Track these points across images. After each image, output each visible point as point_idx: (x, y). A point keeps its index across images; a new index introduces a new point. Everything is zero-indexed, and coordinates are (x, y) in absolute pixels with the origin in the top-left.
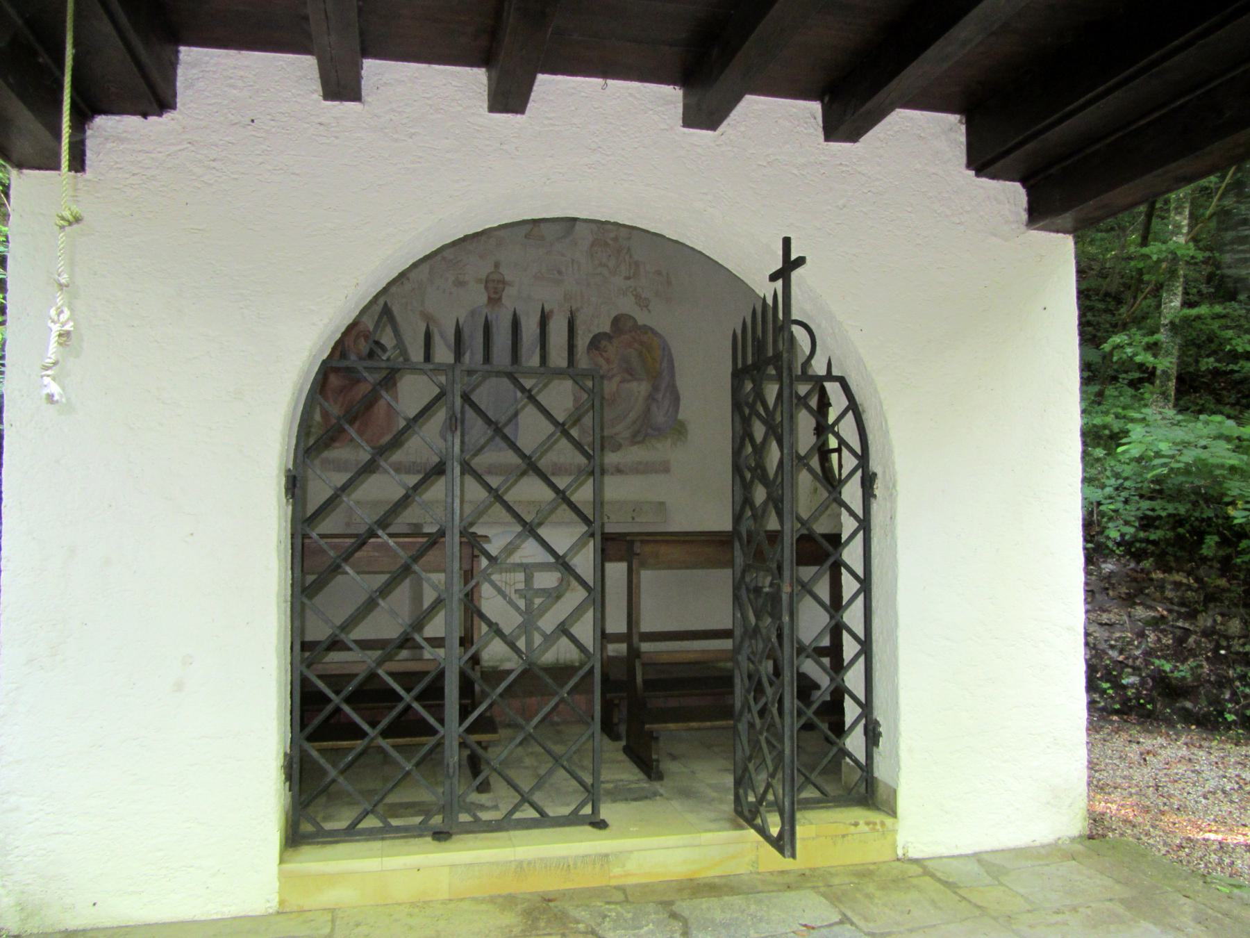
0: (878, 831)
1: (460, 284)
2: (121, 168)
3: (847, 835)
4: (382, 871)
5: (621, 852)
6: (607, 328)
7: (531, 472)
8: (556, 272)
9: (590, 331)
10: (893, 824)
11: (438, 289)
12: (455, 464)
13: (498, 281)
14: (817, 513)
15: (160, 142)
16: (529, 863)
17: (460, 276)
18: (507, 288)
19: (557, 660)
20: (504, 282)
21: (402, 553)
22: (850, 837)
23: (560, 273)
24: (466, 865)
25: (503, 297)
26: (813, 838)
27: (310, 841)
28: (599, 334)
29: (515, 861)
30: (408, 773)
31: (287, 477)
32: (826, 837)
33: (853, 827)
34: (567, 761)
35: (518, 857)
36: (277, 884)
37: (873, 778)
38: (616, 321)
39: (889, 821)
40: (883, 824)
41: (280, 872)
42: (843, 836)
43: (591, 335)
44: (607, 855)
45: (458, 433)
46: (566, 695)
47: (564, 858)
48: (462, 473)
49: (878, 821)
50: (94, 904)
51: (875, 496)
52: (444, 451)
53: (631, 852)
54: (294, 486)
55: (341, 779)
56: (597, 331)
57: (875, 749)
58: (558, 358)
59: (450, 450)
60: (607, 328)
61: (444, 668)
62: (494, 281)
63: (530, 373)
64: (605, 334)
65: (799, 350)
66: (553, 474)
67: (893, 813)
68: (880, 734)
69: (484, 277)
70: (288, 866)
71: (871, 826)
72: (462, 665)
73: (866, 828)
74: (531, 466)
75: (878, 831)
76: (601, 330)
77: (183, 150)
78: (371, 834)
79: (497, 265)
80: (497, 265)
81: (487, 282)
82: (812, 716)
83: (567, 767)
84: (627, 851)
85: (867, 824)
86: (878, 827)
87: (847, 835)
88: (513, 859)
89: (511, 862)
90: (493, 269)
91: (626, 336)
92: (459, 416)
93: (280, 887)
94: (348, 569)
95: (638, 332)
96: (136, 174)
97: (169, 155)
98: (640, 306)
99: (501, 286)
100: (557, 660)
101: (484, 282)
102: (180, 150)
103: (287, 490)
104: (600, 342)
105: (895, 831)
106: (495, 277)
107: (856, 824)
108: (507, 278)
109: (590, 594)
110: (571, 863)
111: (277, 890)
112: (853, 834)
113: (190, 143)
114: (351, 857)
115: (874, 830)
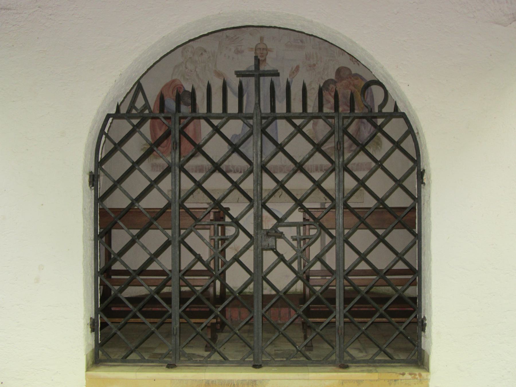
0: (417, 379)
1: (238, 52)
2: (8, 23)
3: (398, 380)
4: (136, 379)
5: (263, 380)
6: (333, 76)
7: (299, 171)
8: (299, 41)
9: (322, 79)
10: (427, 375)
11: (229, 57)
12: (176, 168)
13: (263, 49)
14: (413, 197)
15: (25, 8)
16: (213, 381)
17: (238, 47)
18: (269, 52)
19: (296, 290)
20: (267, 49)
21: (148, 216)
22: (399, 381)
23: (302, 41)
24: (179, 380)
25: (267, 58)
26: (377, 380)
27: (106, 363)
28: (328, 80)
29: (205, 380)
30: (153, 333)
31: (90, 176)
32: (385, 380)
33: (401, 376)
34: (239, 330)
35: (207, 378)
36: (85, 381)
37: (421, 349)
38: (339, 71)
39: (424, 374)
40: (420, 375)
41: (86, 375)
42: (395, 380)
43: (324, 81)
44: (255, 381)
45: (178, 151)
46: (238, 295)
47: (231, 380)
48: (180, 172)
49: (417, 373)
50: (2, 383)
51: (424, 184)
52: (170, 161)
53: (269, 380)
54: (93, 180)
55: (119, 333)
56: (327, 79)
57: (423, 333)
58: (233, 108)
59: (174, 160)
60: (333, 76)
61: (171, 277)
62: (260, 49)
63: (218, 117)
64: (332, 80)
65: (389, 95)
66: (274, 173)
67: (427, 370)
68: (426, 324)
69: (254, 47)
70: (90, 373)
71: (413, 376)
72: (180, 276)
73: (410, 377)
74: (217, 167)
75: (417, 379)
76: (330, 78)
77: (36, 11)
78: (134, 361)
79: (262, 39)
80: (262, 39)
81: (256, 50)
82: (383, 312)
83: (239, 334)
84: (267, 380)
85: (410, 374)
86: (417, 376)
87: (398, 380)
88: (204, 379)
89: (203, 380)
90: (259, 42)
91: (345, 81)
92: (178, 141)
93: (86, 383)
94: (121, 224)
95: (353, 78)
96: (15, 25)
97: (30, 14)
98: (353, 61)
99: (265, 52)
100: (296, 290)
101: (254, 50)
102: (34, 11)
103: (90, 182)
104: (329, 86)
105: (428, 380)
106: (261, 46)
107: (403, 374)
108: (268, 47)
109: (193, 231)
110: (235, 384)
111: (85, 384)
112: (401, 380)
113: (39, 7)
114: (122, 371)
115: (414, 378)
